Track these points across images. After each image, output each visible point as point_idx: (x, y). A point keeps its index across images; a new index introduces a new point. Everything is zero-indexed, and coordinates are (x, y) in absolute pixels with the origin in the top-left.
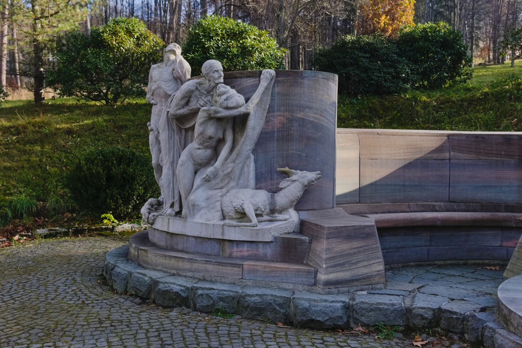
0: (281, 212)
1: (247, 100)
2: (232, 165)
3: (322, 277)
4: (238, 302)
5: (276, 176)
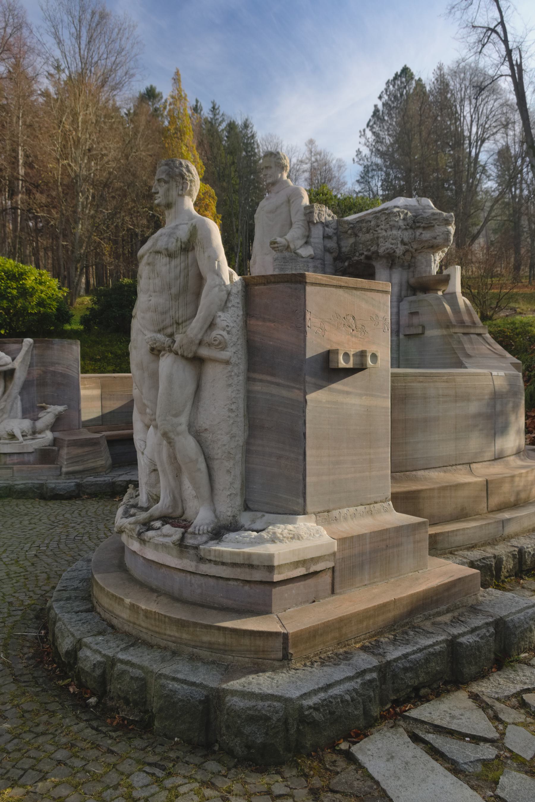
0: (40, 433)
1: (13, 359)
2: (4, 403)
3: (64, 470)
4: (10, 489)
5: (36, 410)
